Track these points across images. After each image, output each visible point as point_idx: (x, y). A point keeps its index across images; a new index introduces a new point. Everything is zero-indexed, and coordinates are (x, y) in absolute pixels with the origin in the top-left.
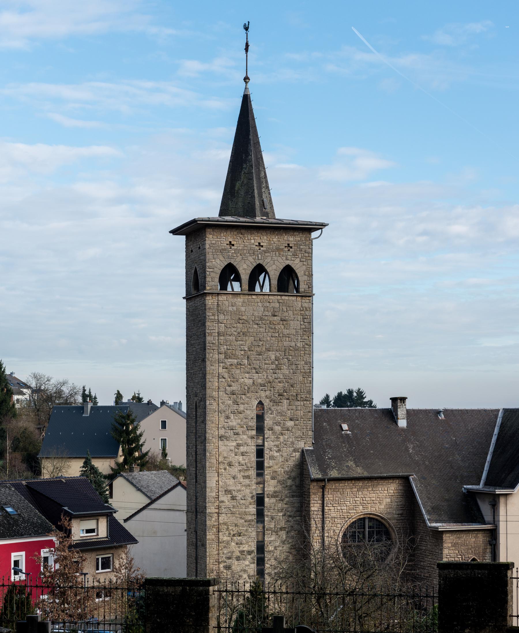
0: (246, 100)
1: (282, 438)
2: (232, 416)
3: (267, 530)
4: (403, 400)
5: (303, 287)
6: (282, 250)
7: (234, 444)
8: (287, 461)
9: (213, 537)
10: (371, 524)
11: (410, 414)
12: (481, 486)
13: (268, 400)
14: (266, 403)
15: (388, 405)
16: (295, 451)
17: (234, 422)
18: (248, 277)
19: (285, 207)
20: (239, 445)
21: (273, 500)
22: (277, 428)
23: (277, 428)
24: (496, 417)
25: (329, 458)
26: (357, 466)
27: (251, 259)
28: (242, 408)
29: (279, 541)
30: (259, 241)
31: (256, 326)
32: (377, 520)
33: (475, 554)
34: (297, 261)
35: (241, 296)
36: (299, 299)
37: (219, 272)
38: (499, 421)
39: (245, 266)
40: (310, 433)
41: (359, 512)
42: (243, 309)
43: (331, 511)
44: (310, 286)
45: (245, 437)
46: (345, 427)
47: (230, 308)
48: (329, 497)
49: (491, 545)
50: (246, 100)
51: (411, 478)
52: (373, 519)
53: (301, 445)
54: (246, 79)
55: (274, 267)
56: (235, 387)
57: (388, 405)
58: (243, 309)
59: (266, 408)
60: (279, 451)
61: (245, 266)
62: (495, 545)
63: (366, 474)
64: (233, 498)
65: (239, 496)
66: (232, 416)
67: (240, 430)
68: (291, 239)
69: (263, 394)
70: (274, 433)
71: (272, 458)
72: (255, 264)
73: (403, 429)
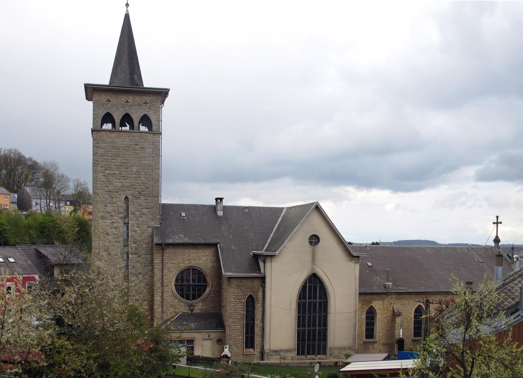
0: (127, 18)
1: (140, 219)
2: (109, 205)
3: (131, 274)
4: (221, 199)
5: (154, 128)
6: (141, 105)
7: (110, 221)
8: (143, 233)
9: (159, 285)
10: (194, 272)
11: (225, 208)
12: (263, 252)
13: (131, 196)
14: (130, 197)
15: (214, 203)
16: (148, 227)
17: (110, 209)
18: (119, 121)
19: (149, 81)
20: (113, 223)
21: (135, 256)
22: (137, 213)
23: (137, 213)
24: (281, 212)
25: (169, 232)
26: (185, 237)
27: (121, 110)
28: (115, 200)
29: (138, 281)
30: (127, 99)
31: (124, 151)
32: (198, 270)
33: (252, 292)
34: (151, 112)
35: (115, 132)
36: (152, 135)
37: (101, 117)
38: (283, 214)
39: (117, 114)
40: (159, 217)
41: (183, 266)
42: (116, 140)
43: (168, 265)
44: (159, 126)
45: (117, 217)
46: (183, 214)
47: (108, 140)
48: (166, 255)
49: (262, 287)
50: (127, 18)
51: (218, 245)
52: (196, 269)
53: (153, 224)
54: (127, 5)
55: (136, 115)
56: (111, 188)
57: (214, 203)
58: (116, 140)
59: (130, 201)
60: (138, 227)
61: (117, 114)
62: (264, 287)
63: (187, 240)
64: (109, 254)
65: (113, 253)
66: (109, 205)
67: (113, 214)
68: (147, 98)
69: (128, 192)
70: (136, 216)
71: (134, 231)
72: (124, 113)
73: (220, 217)
